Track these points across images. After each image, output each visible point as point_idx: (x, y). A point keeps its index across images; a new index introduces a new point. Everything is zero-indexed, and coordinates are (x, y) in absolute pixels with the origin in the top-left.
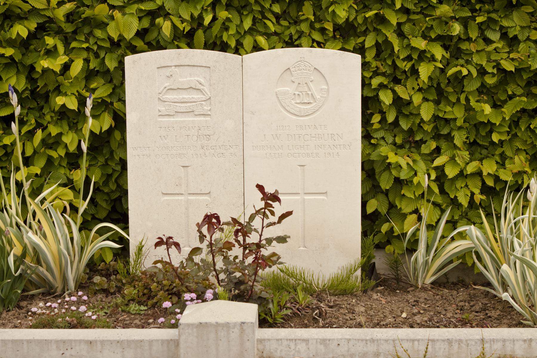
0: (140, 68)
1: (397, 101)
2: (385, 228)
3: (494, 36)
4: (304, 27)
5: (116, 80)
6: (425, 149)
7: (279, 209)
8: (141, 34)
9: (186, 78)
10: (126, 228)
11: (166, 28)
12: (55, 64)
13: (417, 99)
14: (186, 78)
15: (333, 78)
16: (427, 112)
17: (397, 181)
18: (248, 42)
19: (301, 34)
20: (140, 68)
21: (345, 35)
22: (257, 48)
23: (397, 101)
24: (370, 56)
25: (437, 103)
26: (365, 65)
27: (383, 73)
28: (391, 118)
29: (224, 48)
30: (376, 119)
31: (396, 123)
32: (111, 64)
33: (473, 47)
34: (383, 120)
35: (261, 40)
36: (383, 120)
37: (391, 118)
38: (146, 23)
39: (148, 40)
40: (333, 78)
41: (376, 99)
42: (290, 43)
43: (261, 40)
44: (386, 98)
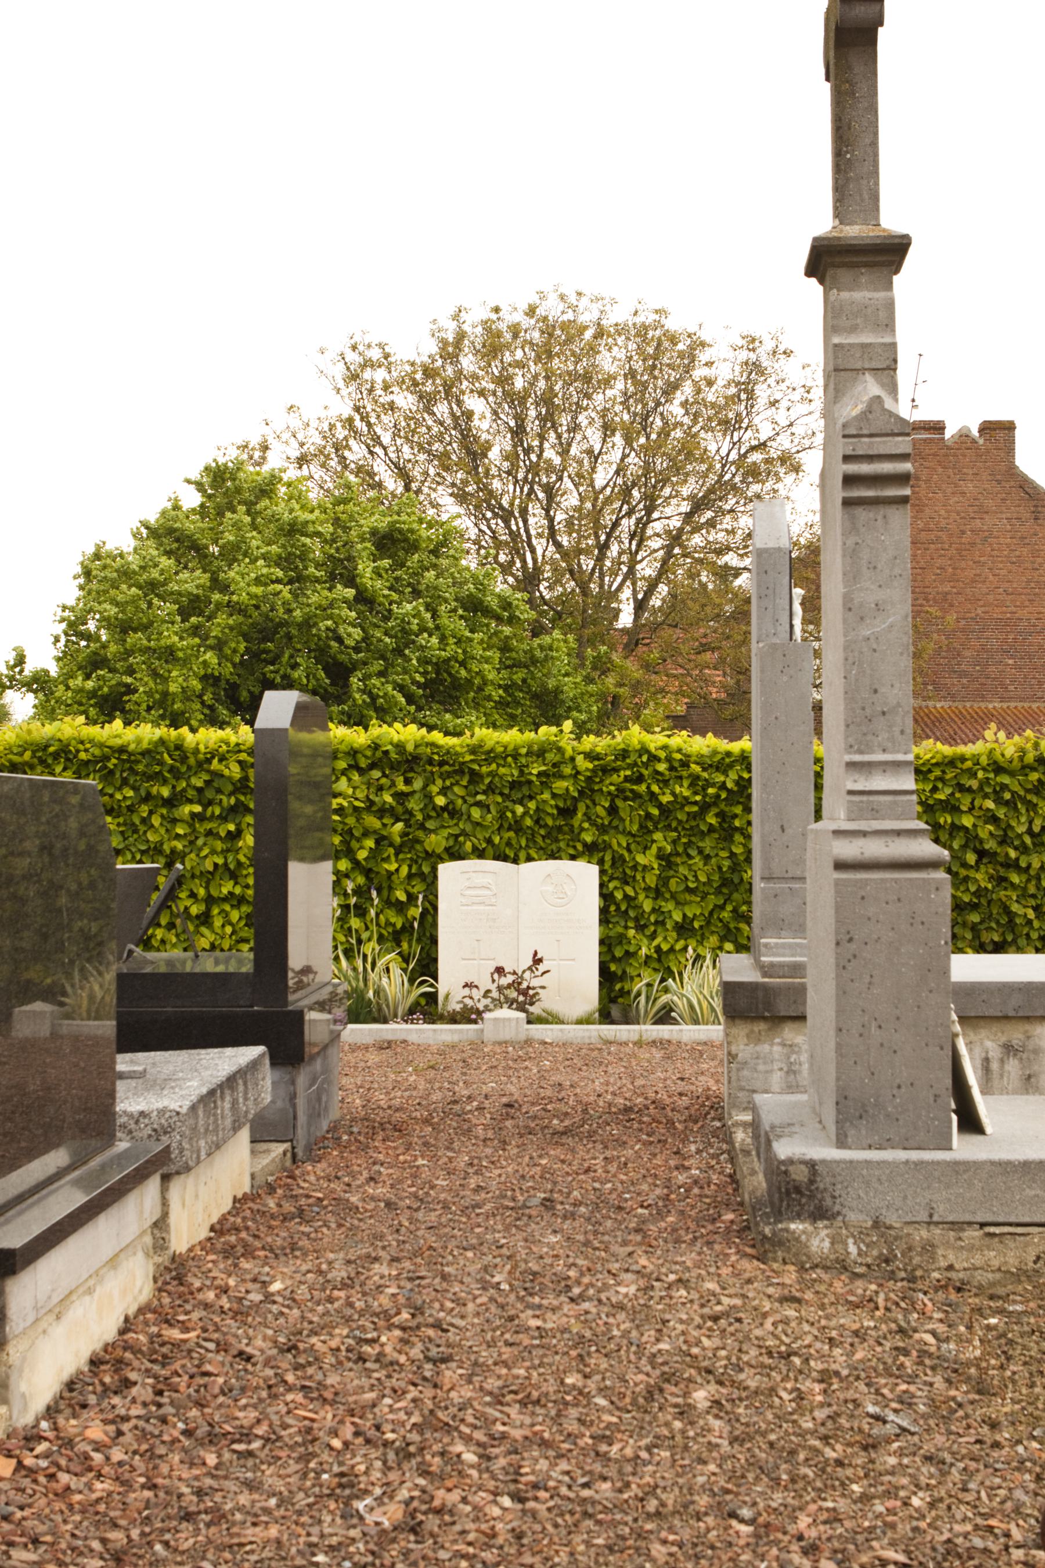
0: (449, 873)
1: (626, 896)
2: (618, 987)
3: (693, 852)
4: (562, 845)
5: (431, 882)
6: (648, 932)
7: (542, 968)
8: (447, 849)
9: (480, 880)
10: (436, 979)
11: (468, 846)
12: (393, 867)
13: (641, 897)
14: (480, 880)
15: (579, 881)
16: (647, 906)
17: (627, 952)
18: (522, 855)
19: (559, 849)
20: (449, 873)
21: (590, 851)
22: (529, 859)
23: (626, 896)
24: (607, 866)
25: (655, 899)
26: (602, 872)
27: (615, 874)
28: (623, 908)
29: (505, 858)
30: (613, 908)
31: (626, 912)
32: (426, 869)
33: (679, 860)
34: (618, 909)
35: (533, 853)
36: (618, 909)
37: (623, 908)
38: (451, 842)
39: (455, 854)
40: (579, 881)
41: (612, 894)
42: (553, 856)
43: (533, 853)
44: (619, 895)
